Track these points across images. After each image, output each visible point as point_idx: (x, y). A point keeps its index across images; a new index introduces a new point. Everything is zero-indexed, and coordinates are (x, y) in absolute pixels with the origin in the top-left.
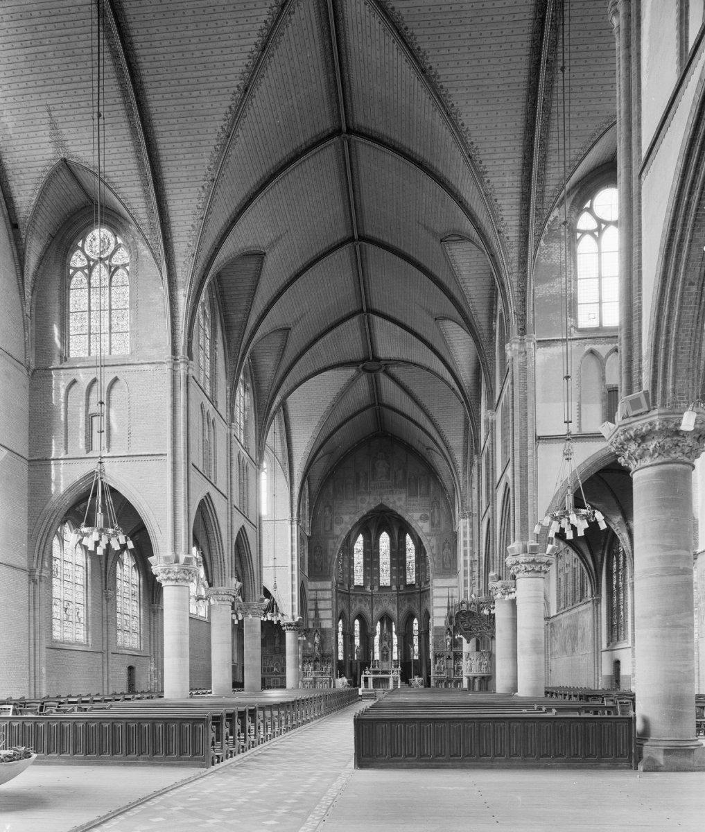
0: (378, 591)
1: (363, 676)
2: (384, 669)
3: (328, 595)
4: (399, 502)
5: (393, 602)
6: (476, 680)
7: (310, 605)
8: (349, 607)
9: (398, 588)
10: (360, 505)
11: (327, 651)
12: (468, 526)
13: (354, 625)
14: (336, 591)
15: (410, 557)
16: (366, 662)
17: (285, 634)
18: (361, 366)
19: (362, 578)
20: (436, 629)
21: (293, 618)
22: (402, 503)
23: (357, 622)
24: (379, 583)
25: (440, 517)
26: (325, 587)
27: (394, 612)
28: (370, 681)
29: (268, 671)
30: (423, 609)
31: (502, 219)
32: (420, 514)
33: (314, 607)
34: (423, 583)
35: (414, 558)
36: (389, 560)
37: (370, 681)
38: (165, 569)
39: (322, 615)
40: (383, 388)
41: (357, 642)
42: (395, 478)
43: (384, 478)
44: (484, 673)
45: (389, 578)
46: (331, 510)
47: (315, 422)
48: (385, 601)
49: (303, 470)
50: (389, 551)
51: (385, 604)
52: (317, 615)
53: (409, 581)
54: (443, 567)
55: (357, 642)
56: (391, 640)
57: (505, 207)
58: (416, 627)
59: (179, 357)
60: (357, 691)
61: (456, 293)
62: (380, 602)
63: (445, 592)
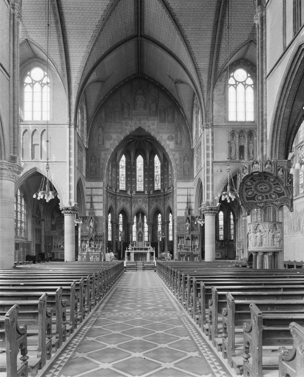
1: (127, 251)
2: (140, 247)
3: (101, 192)
5: (145, 202)
6: (266, 257)
7: (87, 199)
8: (116, 204)
9: (149, 192)
10: (125, 127)
11: (99, 233)
13: (119, 217)
14: (107, 191)
15: (157, 172)
16: (127, 242)
17: (64, 217)
19: (125, 185)
20: (179, 218)
21: (70, 203)
22: (155, 127)
23: (121, 215)
26: (98, 186)
27: (146, 208)
28: (132, 255)
29: (57, 247)
30: (166, 207)
32: (168, 135)
33: (89, 200)
34: (166, 189)
35: (160, 173)
36: (143, 174)
37: (132, 255)
39: (96, 206)
41: (121, 228)
42: (150, 109)
43: (142, 109)
44: (276, 246)
45: (143, 186)
46: (103, 130)
48: (140, 201)
49: (79, 82)
50: (143, 168)
51: (140, 203)
52: (92, 206)
53: (156, 188)
54: (184, 174)
55: (121, 228)
56: (143, 227)
58: (160, 220)
60: (123, 263)
62: (137, 202)
63: (185, 192)
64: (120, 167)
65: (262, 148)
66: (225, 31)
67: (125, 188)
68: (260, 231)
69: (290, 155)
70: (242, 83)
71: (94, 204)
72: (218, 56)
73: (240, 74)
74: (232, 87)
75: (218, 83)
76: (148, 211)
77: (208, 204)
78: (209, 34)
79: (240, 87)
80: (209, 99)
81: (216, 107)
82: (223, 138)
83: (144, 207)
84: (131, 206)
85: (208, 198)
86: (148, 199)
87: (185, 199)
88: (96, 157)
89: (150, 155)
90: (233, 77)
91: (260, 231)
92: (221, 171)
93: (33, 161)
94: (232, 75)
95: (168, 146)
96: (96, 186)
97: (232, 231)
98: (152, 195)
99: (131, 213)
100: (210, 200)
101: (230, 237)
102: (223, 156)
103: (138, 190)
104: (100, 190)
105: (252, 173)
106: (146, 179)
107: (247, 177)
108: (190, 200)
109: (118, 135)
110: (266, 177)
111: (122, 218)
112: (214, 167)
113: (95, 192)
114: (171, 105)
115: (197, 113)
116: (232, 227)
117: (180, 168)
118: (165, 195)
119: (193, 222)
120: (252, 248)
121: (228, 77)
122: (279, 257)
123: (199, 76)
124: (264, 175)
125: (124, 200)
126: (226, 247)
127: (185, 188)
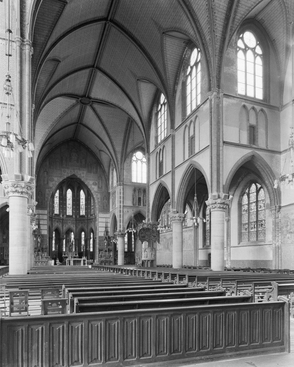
0: (66, 218)
3: (46, 217)
4: (82, 174)
6: (149, 262)
8: (52, 224)
9: (76, 217)
10: (63, 173)
12: (122, 189)
15: (82, 202)
18: (80, 99)
20: (100, 237)
22: (84, 175)
24: (66, 214)
25: (102, 184)
26: (44, 213)
27: (73, 227)
30: (89, 228)
31: (216, 24)
32: (93, 182)
34: (89, 216)
35: (84, 203)
38: (15, 184)
39: (42, 227)
40: (86, 115)
42: (81, 162)
44: (153, 258)
45: (71, 212)
46: (47, 174)
47: (49, 124)
48: (69, 223)
50: (71, 199)
51: (69, 224)
53: (81, 214)
54: (103, 208)
57: (218, 19)
59: (25, 40)
61: (160, 66)
62: (67, 223)
63: (104, 220)
64: (55, 197)
65: (148, 215)
66: (131, 134)
67: (58, 212)
68: (146, 252)
69: (159, 220)
70: (140, 160)
71: (41, 226)
72: (127, 146)
73: (139, 155)
74: (134, 162)
75: (127, 159)
76: (75, 230)
77: (120, 231)
78: (123, 135)
79: (139, 162)
80: (122, 168)
81: (125, 173)
82: (129, 192)
83: (73, 227)
84: (63, 226)
85: (120, 227)
86: (75, 222)
87: (104, 225)
88: (42, 193)
89: (77, 190)
90: (135, 156)
91: (146, 252)
92: (128, 212)
93: (5, 197)
94: (134, 154)
95: (93, 189)
96: (42, 213)
97: (133, 246)
98: (78, 218)
99: (63, 231)
100: (122, 229)
101: (132, 250)
102: (129, 203)
103: (67, 214)
104: (45, 216)
105: (144, 228)
106: (74, 207)
107: (142, 229)
108: (107, 226)
109: (59, 178)
110: (149, 230)
111: (54, 234)
112: (124, 209)
113: (41, 217)
114: (94, 161)
115: (113, 170)
116: (133, 243)
117: (101, 204)
118: (88, 220)
119: (109, 240)
120: (143, 259)
121: (132, 156)
122: (154, 262)
123: (116, 155)
124: (148, 229)
125: (57, 222)
126: (130, 257)
127: (104, 218)
